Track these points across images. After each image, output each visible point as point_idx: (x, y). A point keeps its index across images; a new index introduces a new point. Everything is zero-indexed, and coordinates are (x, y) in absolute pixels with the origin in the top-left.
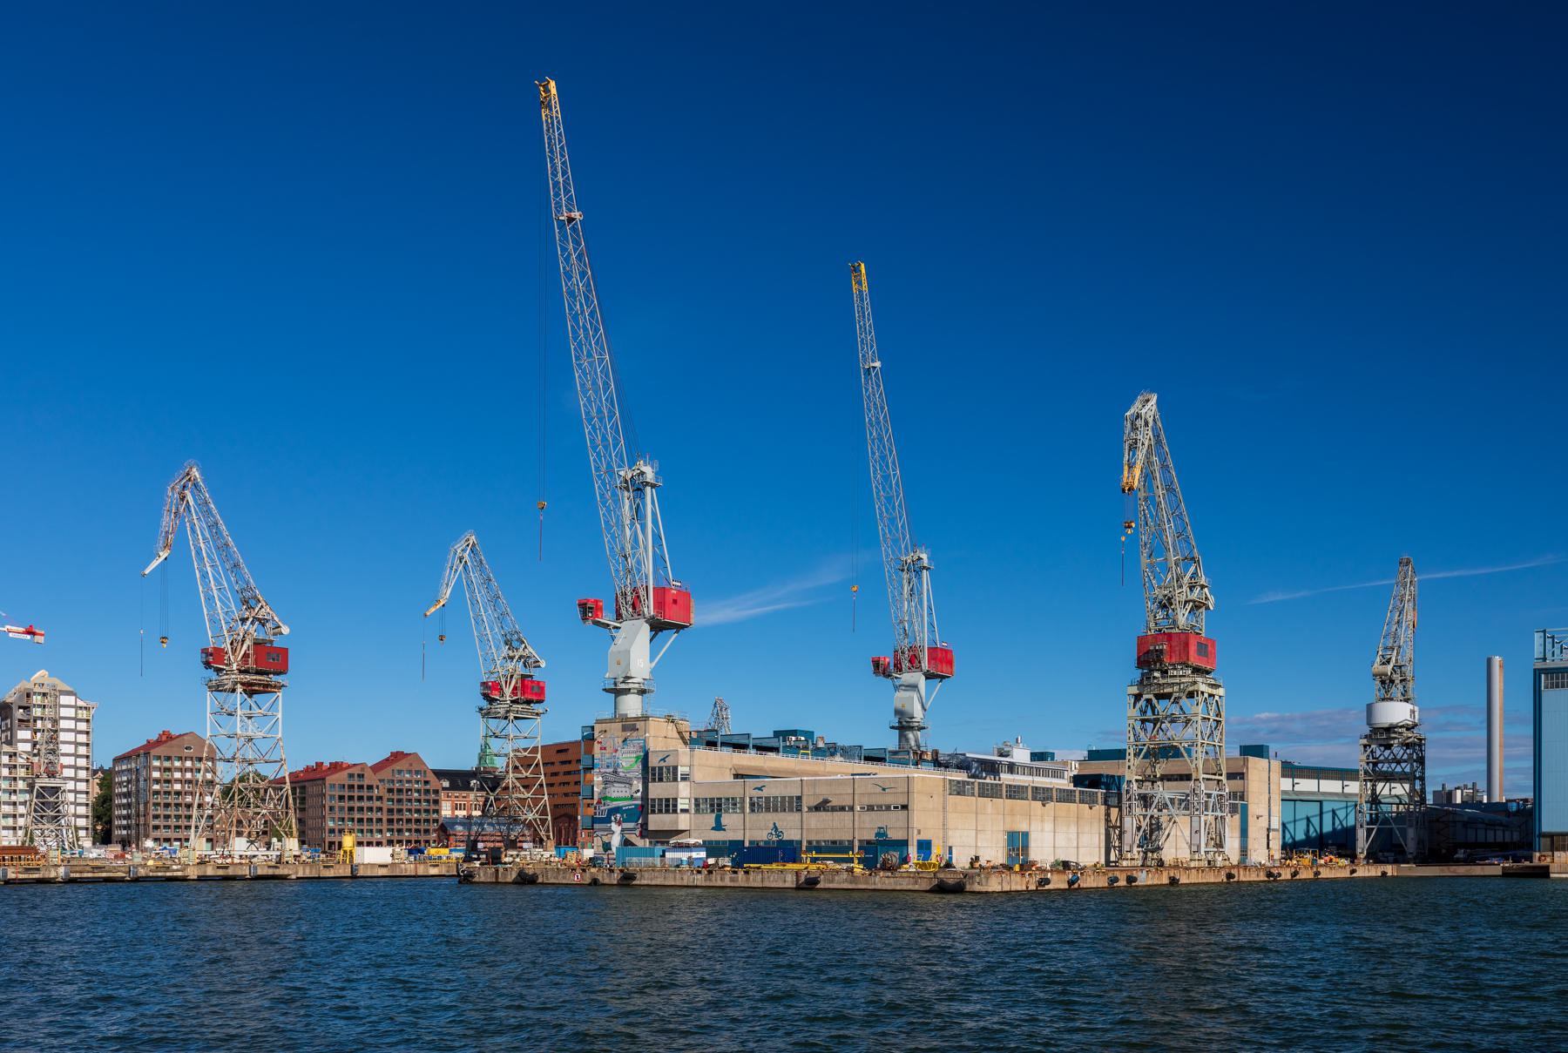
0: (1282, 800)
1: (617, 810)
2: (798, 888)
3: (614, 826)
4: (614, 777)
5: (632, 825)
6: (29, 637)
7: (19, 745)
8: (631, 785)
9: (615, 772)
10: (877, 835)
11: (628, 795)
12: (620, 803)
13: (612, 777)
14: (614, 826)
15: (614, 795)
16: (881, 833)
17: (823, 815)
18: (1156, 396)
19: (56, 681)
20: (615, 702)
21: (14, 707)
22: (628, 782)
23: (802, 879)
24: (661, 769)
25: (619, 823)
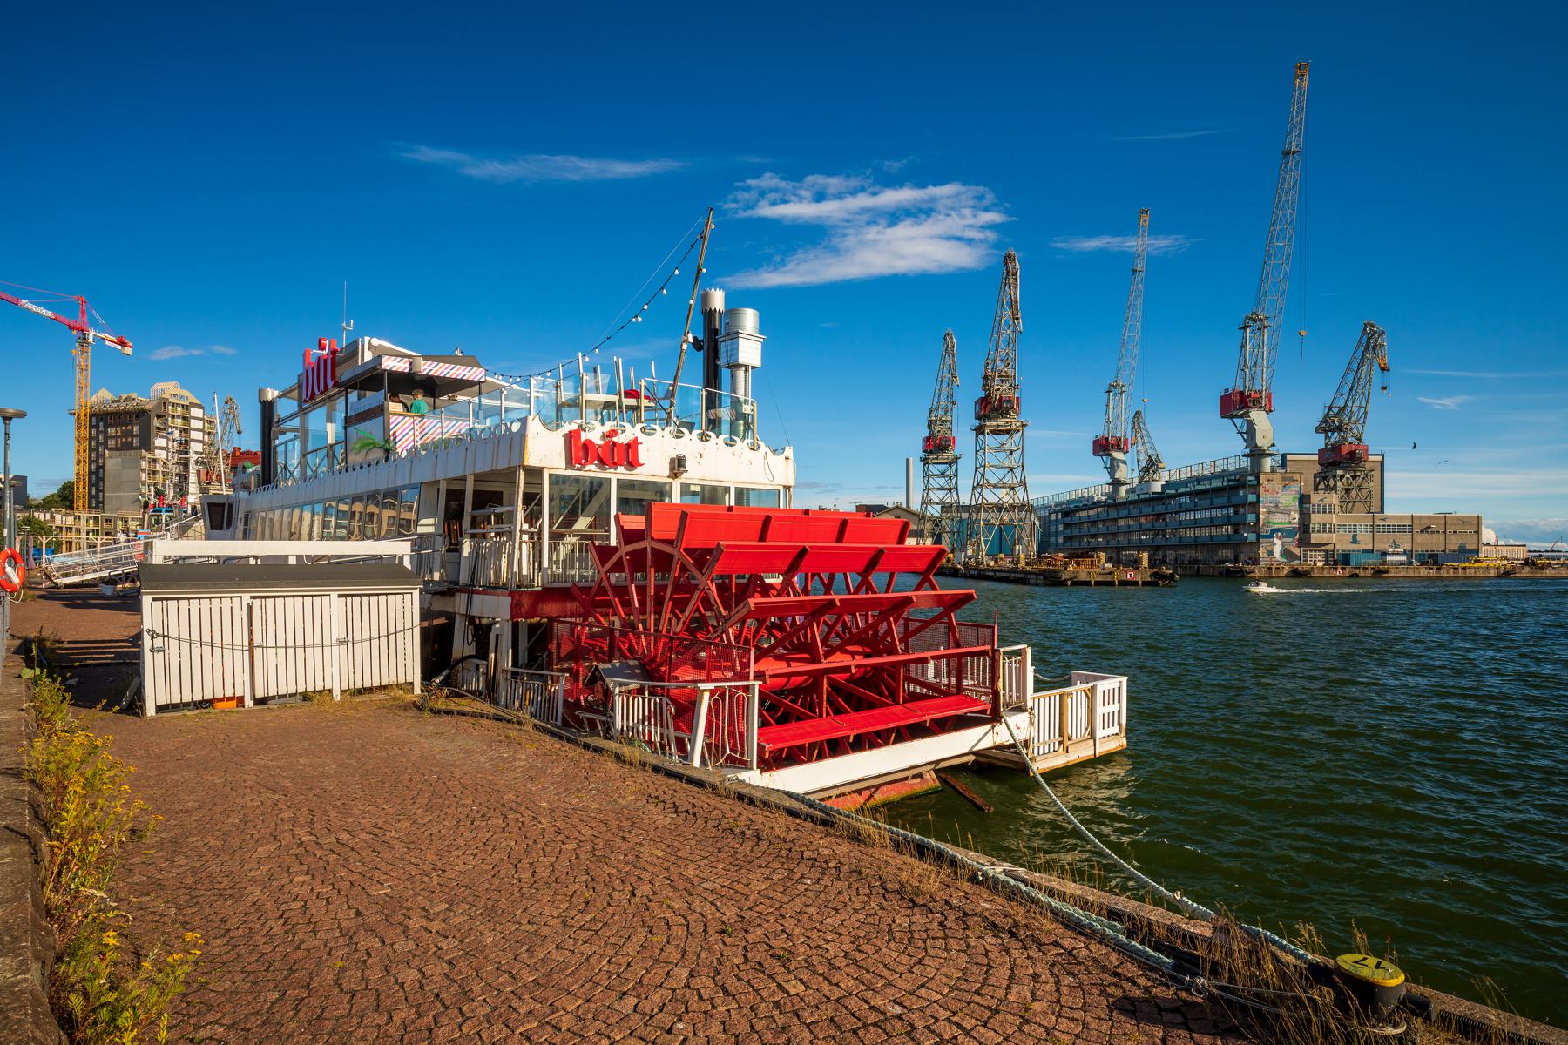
0: (767, 520)
1: (1278, 530)
2: (1498, 577)
3: (1275, 540)
4: (1277, 508)
5: (1290, 540)
6: (120, 347)
7: (157, 451)
8: (1289, 514)
9: (1277, 506)
10: (1460, 547)
11: (1287, 521)
12: (1280, 526)
13: (1274, 510)
14: (1275, 540)
15: (1275, 521)
16: (1462, 546)
17: (1426, 535)
18: (24, 302)
19: (186, 393)
20: (6, 444)
21: (153, 415)
22: (1287, 513)
23: (1502, 571)
24: (1319, 505)
25: (1280, 539)
